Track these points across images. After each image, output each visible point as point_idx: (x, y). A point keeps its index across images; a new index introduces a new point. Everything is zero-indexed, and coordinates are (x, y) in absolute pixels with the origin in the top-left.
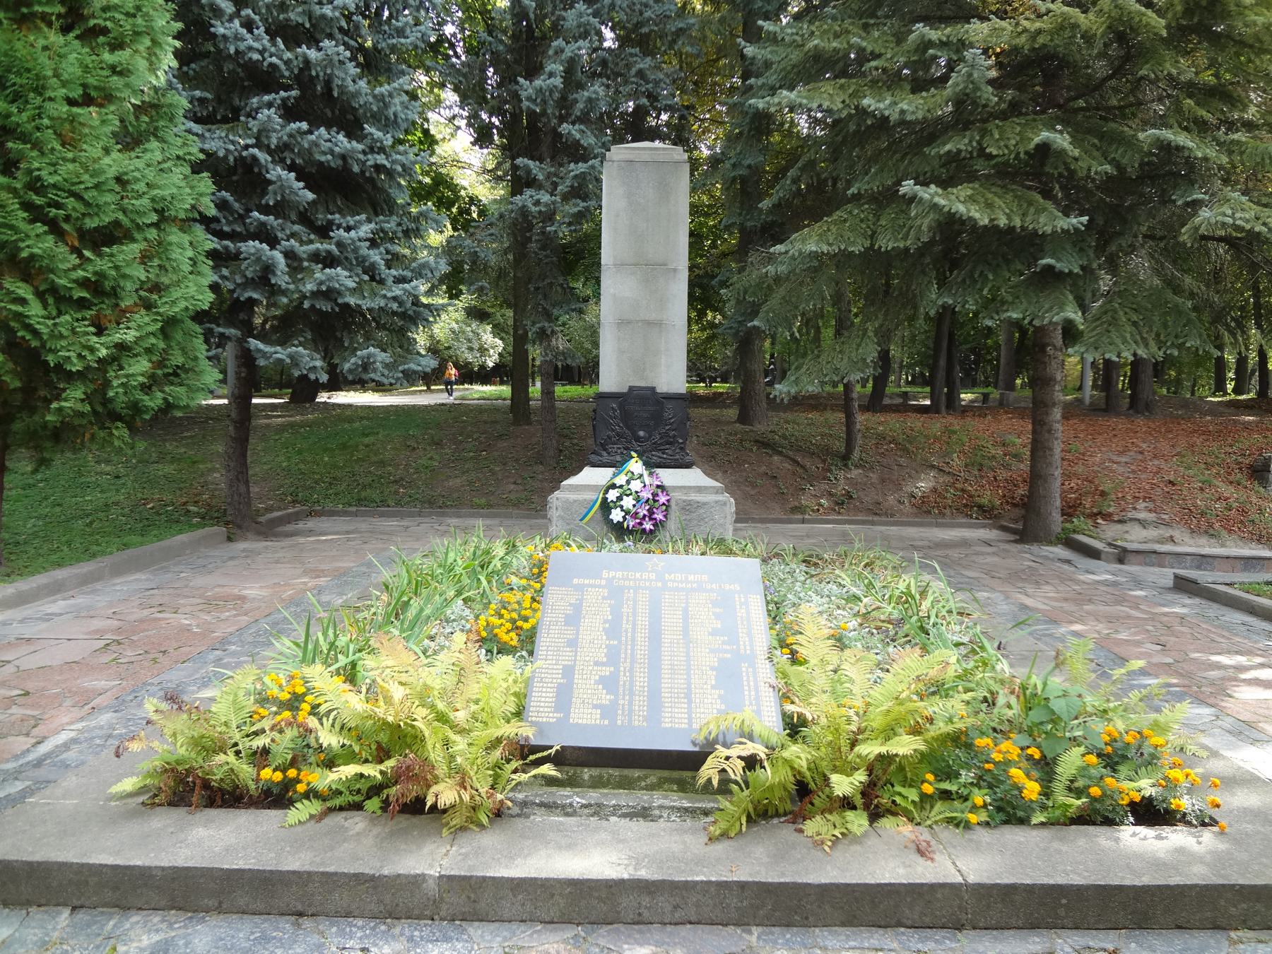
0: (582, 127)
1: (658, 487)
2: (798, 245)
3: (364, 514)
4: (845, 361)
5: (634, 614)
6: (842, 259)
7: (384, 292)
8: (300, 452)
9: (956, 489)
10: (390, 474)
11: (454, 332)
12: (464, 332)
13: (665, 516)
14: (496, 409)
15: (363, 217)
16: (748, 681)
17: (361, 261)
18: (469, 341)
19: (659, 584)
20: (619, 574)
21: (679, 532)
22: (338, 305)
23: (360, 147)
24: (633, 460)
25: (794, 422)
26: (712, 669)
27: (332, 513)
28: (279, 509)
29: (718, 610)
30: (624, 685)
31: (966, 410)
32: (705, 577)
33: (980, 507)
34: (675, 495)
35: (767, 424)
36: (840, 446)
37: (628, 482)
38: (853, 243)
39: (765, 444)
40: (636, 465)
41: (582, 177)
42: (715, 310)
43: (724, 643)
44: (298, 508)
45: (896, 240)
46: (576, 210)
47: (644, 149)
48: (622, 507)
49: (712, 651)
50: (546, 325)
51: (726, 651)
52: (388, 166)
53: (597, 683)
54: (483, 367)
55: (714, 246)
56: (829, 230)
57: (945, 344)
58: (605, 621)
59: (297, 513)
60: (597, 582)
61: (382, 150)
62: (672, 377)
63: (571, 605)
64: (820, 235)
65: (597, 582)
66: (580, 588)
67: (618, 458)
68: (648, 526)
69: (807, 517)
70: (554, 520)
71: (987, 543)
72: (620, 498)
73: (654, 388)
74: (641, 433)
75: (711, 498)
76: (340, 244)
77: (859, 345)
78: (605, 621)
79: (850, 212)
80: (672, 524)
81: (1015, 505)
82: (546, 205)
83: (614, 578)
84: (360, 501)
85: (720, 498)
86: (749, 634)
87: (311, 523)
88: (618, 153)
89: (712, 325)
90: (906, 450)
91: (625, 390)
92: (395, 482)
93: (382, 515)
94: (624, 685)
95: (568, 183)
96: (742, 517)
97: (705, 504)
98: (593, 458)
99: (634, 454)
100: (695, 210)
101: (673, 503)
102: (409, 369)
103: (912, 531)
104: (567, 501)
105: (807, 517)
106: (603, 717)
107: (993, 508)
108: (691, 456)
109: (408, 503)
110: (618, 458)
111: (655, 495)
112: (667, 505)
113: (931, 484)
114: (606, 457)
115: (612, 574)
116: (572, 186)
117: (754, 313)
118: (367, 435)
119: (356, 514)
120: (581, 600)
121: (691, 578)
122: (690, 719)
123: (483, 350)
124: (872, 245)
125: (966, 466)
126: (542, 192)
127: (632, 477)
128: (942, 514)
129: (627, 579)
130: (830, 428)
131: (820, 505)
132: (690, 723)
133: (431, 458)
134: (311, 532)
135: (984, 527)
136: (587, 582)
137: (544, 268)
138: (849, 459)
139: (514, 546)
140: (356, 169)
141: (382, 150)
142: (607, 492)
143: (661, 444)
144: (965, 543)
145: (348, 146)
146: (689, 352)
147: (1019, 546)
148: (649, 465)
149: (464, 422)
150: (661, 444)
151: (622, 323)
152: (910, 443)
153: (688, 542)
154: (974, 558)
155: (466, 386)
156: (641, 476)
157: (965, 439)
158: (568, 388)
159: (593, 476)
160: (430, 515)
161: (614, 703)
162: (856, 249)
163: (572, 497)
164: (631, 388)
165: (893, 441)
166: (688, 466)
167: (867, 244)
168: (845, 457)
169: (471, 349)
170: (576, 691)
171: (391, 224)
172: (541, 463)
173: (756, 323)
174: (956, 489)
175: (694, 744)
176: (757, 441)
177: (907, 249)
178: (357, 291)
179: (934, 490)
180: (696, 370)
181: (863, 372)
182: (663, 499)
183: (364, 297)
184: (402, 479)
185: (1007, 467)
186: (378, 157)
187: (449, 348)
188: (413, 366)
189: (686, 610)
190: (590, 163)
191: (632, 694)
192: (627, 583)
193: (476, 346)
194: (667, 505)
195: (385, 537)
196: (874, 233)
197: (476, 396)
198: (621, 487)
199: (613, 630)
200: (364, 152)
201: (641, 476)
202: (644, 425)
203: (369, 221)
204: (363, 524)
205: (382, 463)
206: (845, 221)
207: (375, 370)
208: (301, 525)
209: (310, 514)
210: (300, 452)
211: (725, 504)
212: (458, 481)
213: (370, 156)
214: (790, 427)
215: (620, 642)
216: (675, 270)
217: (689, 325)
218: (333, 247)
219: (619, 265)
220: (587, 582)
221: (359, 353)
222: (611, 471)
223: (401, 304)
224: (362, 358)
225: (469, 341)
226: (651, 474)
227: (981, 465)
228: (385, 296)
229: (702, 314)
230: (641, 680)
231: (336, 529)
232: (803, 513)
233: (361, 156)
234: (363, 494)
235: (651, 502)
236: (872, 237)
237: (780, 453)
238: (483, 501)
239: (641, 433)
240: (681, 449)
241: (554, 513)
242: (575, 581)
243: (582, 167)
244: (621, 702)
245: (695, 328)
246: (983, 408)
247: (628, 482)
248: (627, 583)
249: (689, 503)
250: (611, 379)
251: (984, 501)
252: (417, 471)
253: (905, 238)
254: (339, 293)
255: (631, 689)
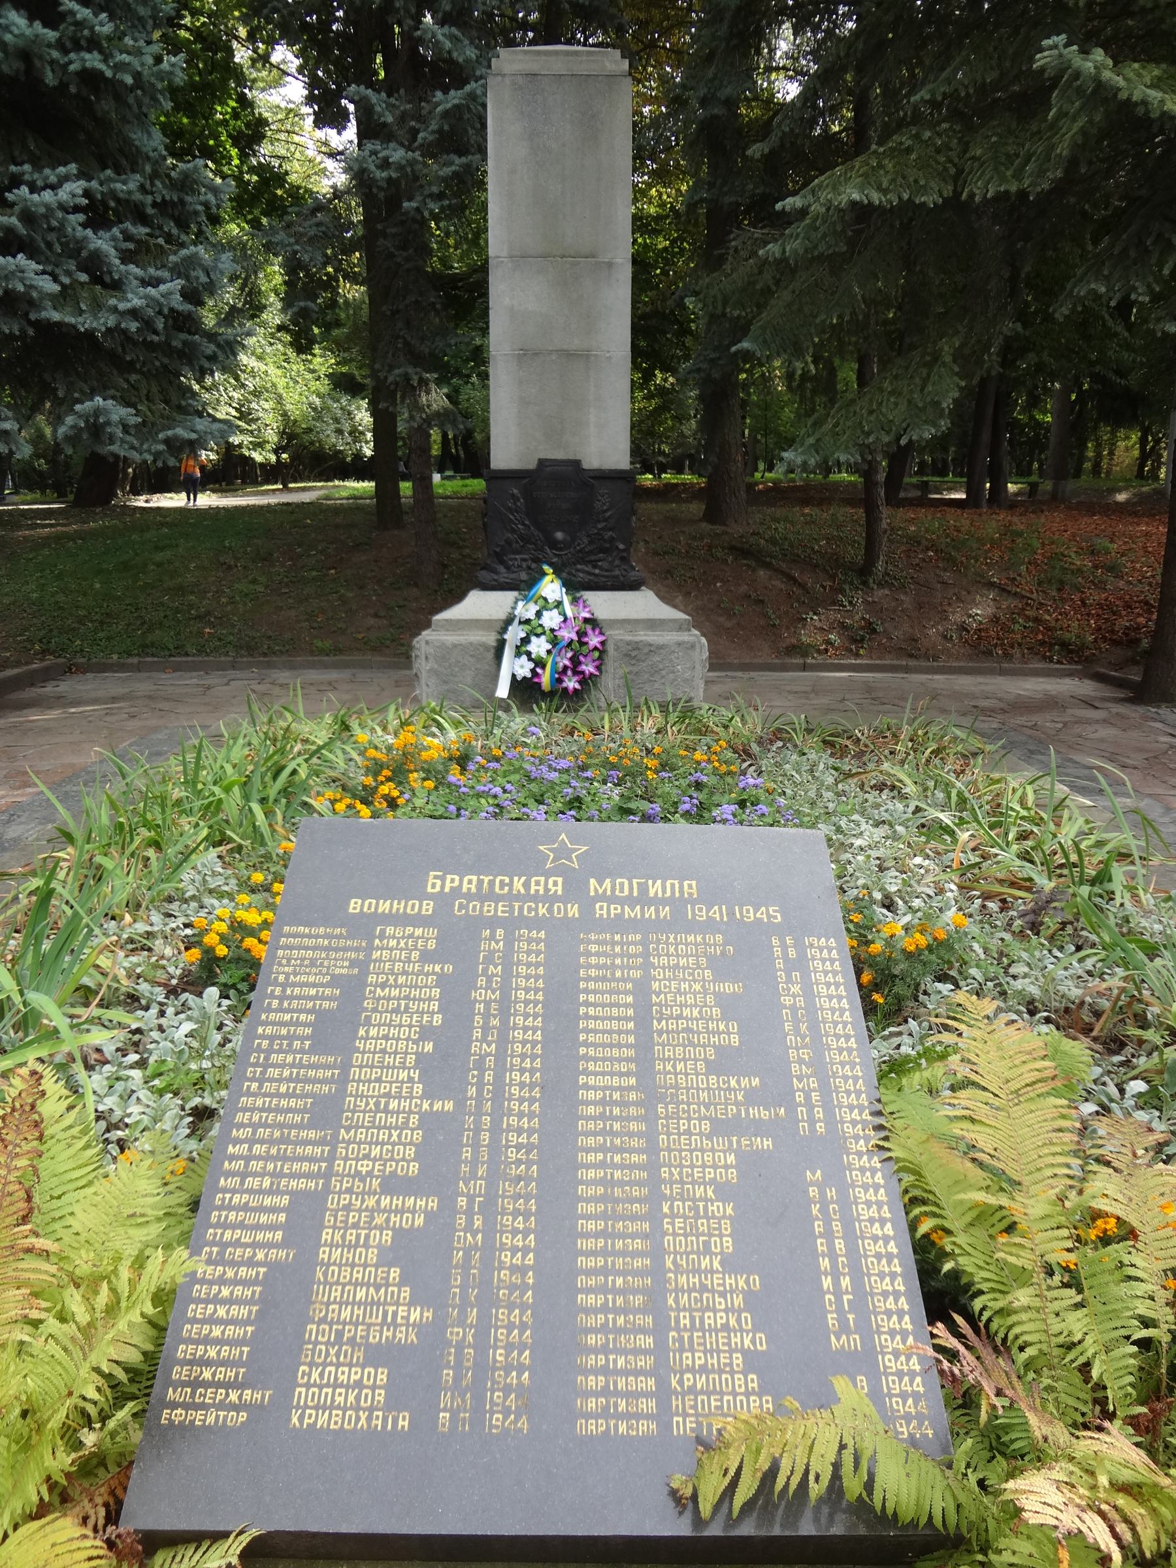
0: (454, 30)
1: (586, 620)
2: (824, 195)
3: (151, 668)
4: (903, 407)
5: (505, 1009)
6: (906, 215)
7: (112, 302)
8: (60, 577)
9: (1027, 618)
10: (191, 606)
11: (315, 409)
12: (328, 409)
13: (598, 668)
14: (360, 508)
15: (73, 168)
16: (829, 1235)
17: (74, 249)
18: (337, 420)
19: (574, 911)
20: (470, 882)
21: (623, 691)
22: (29, 322)
23: (51, 35)
24: (548, 578)
25: (786, 520)
26: (723, 1192)
27: (103, 668)
28: (18, 664)
29: (728, 988)
30: (466, 1265)
31: (1012, 505)
32: (690, 887)
33: (1064, 645)
34: (616, 635)
35: (748, 524)
36: (855, 554)
37: (539, 614)
38: (924, 189)
39: (743, 551)
40: (551, 587)
41: (453, 114)
42: (664, 370)
43: (752, 1097)
44: (50, 660)
45: (1003, 179)
46: (448, 171)
47: (557, 53)
48: (529, 654)
49: (720, 1128)
50: (410, 370)
51: (759, 1129)
52: (109, 74)
53: (387, 1258)
54: (358, 456)
55: (665, 273)
56: (880, 166)
57: (990, 410)
58: (426, 1033)
59: (47, 669)
60: (413, 907)
61: (93, 43)
62: (606, 443)
63: (335, 981)
64: (865, 175)
65: (413, 907)
66: (365, 927)
67: (524, 576)
68: (571, 683)
69: (809, 661)
70: (424, 676)
71: (1089, 704)
72: (526, 641)
73: (576, 463)
74: (559, 535)
75: (669, 637)
76: (28, 217)
77: (925, 381)
78: (426, 1033)
79: (917, 137)
80: (610, 682)
81: (1115, 643)
82: (400, 168)
83: (456, 891)
84: (145, 649)
85: (685, 637)
86: (820, 1067)
87: (65, 687)
88: (512, 61)
89: (662, 391)
90: (951, 560)
91: (532, 465)
92: (199, 618)
93: (177, 668)
94: (466, 1265)
95: (434, 126)
96: (717, 663)
97: (661, 647)
98: (484, 575)
99: (546, 568)
100: (640, 224)
101: (610, 648)
102: (176, 438)
103: (965, 683)
104: (443, 646)
105: (809, 661)
106: (393, 1404)
107: (1083, 647)
108: (638, 570)
109: (216, 649)
110: (524, 576)
111: (581, 634)
112: (602, 650)
113: (990, 611)
114: (504, 575)
115: (452, 881)
116: (440, 131)
117: (741, 329)
118: (162, 549)
119: (138, 668)
120: (363, 966)
121: (655, 888)
122: (663, 1394)
123: (356, 434)
124: (957, 194)
125: (1040, 583)
126: (392, 145)
127: (545, 605)
128: (1007, 656)
129: (492, 896)
130: (839, 527)
131: (829, 642)
132: (663, 1416)
133: (254, 581)
134: (60, 701)
135: (1070, 674)
136: (384, 906)
137: (407, 292)
138: (870, 573)
139: (347, 728)
140: (50, 78)
141: (93, 43)
142: (504, 630)
143: (591, 552)
144: (1050, 704)
145: (28, 32)
146: (632, 428)
147: (1141, 709)
148: (573, 586)
149: (306, 526)
150: (591, 552)
151: (526, 355)
152: (958, 550)
153: (636, 708)
154: (1078, 729)
155: (337, 482)
156: (559, 604)
157: (1036, 544)
158: (468, 482)
159: (482, 605)
160: (249, 666)
161: (433, 1334)
162: (930, 199)
163: (450, 638)
164: (541, 462)
165: (933, 546)
166: (634, 586)
167: (948, 191)
168: (864, 571)
169: (339, 432)
170: (321, 1294)
171: (129, 186)
172: (416, 585)
173: (745, 345)
174: (1027, 618)
175: (685, 1502)
176: (732, 548)
177: (1023, 194)
178: (66, 296)
179: (995, 620)
180: (643, 431)
181: (935, 425)
182: (594, 640)
183: (81, 312)
184: (209, 613)
185: (1100, 585)
186: (87, 56)
187: (309, 430)
188: (180, 431)
189: (642, 990)
190: (468, 88)
191: (488, 1301)
192: (489, 909)
193: (347, 427)
194: (602, 650)
195: (165, 705)
196: (960, 172)
197: (344, 494)
198: (528, 621)
199: (443, 1065)
200: (60, 45)
201: (559, 604)
202: (564, 523)
203: (82, 175)
204: (142, 685)
205: (181, 590)
206: (909, 150)
207: (112, 439)
208: (49, 689)
209: (70, 670)
210: (60, 577)
211: (693, 646)
212: (293, 613)
213: (72, 55)
214: (781, 527)
215: (460, 1104)
216: (610, 265)
217: (632, 392)
218: (14, 220)
219: (520, 257)
220: (384, 906)
221: (78, 407)
222: (511, 595)
223: (148, 325)
224: (85, 417)
225: (337, 420)
226: (575, 601)
227: (1062, 582)
228: (115, 310)
229: (648, 376)
230: (517, 1247)
231: (101, 694)
232: (805, 655)
233: (55, 54)
234: (150, 638)
235: (576, 645)
236: (956, 178)
237: (768, 566)
238: (328, 644)
239: (559, 535)
240: (623, 559)
241: (423, 665)
242: (354, 906)
243: (455, 97)
244: (455, 1333)
245: (639, 395)
246: (1032, 501)
247: (539, 614)
248: (489, 909)
249: (636, 646)
250: (508, 449)
251: (1070, 636)
252: (232, 601)
253: (1018, 175)
254: (32, 303)
255: (485, 1283)
